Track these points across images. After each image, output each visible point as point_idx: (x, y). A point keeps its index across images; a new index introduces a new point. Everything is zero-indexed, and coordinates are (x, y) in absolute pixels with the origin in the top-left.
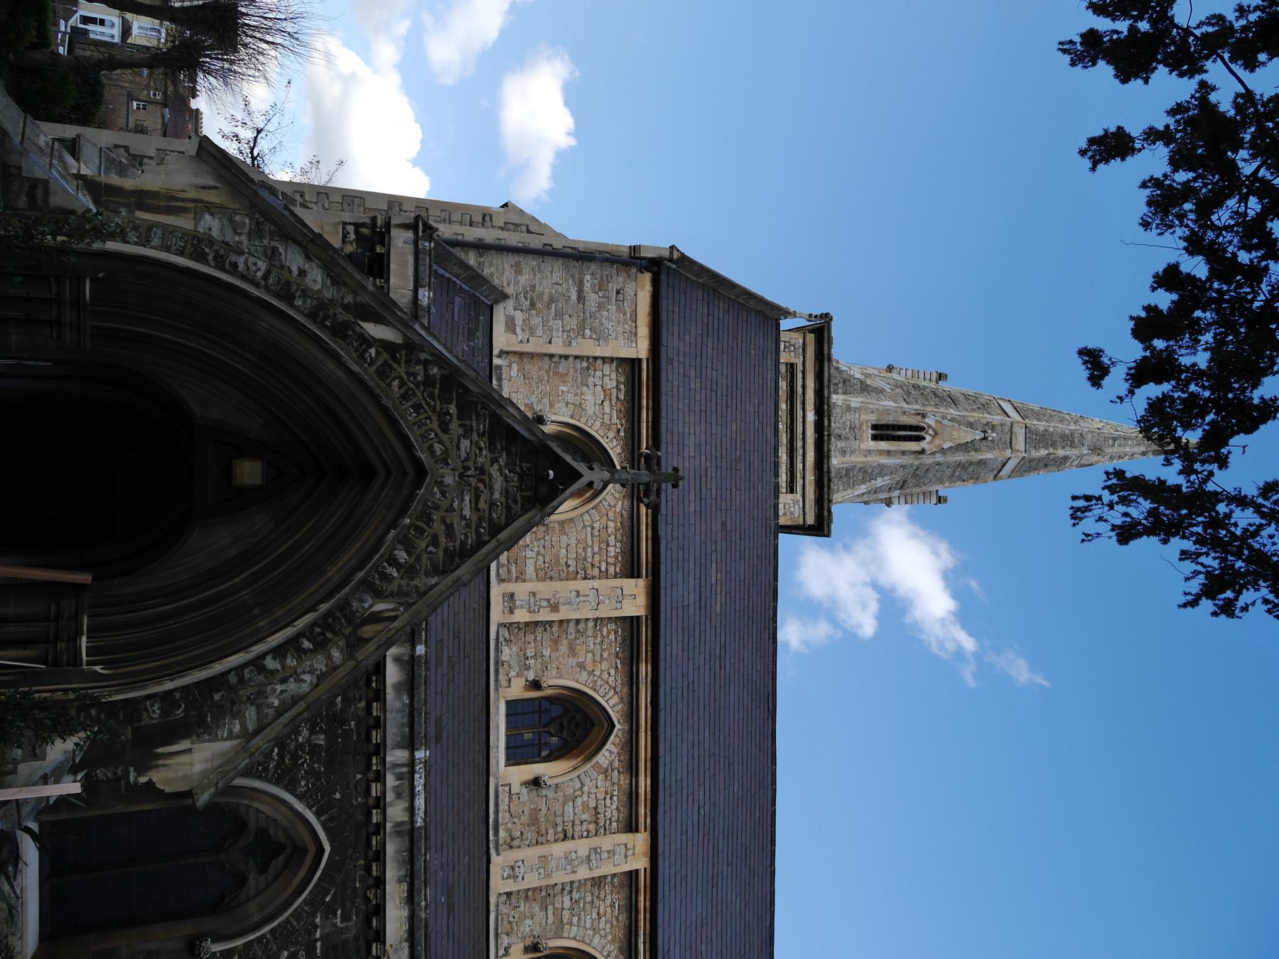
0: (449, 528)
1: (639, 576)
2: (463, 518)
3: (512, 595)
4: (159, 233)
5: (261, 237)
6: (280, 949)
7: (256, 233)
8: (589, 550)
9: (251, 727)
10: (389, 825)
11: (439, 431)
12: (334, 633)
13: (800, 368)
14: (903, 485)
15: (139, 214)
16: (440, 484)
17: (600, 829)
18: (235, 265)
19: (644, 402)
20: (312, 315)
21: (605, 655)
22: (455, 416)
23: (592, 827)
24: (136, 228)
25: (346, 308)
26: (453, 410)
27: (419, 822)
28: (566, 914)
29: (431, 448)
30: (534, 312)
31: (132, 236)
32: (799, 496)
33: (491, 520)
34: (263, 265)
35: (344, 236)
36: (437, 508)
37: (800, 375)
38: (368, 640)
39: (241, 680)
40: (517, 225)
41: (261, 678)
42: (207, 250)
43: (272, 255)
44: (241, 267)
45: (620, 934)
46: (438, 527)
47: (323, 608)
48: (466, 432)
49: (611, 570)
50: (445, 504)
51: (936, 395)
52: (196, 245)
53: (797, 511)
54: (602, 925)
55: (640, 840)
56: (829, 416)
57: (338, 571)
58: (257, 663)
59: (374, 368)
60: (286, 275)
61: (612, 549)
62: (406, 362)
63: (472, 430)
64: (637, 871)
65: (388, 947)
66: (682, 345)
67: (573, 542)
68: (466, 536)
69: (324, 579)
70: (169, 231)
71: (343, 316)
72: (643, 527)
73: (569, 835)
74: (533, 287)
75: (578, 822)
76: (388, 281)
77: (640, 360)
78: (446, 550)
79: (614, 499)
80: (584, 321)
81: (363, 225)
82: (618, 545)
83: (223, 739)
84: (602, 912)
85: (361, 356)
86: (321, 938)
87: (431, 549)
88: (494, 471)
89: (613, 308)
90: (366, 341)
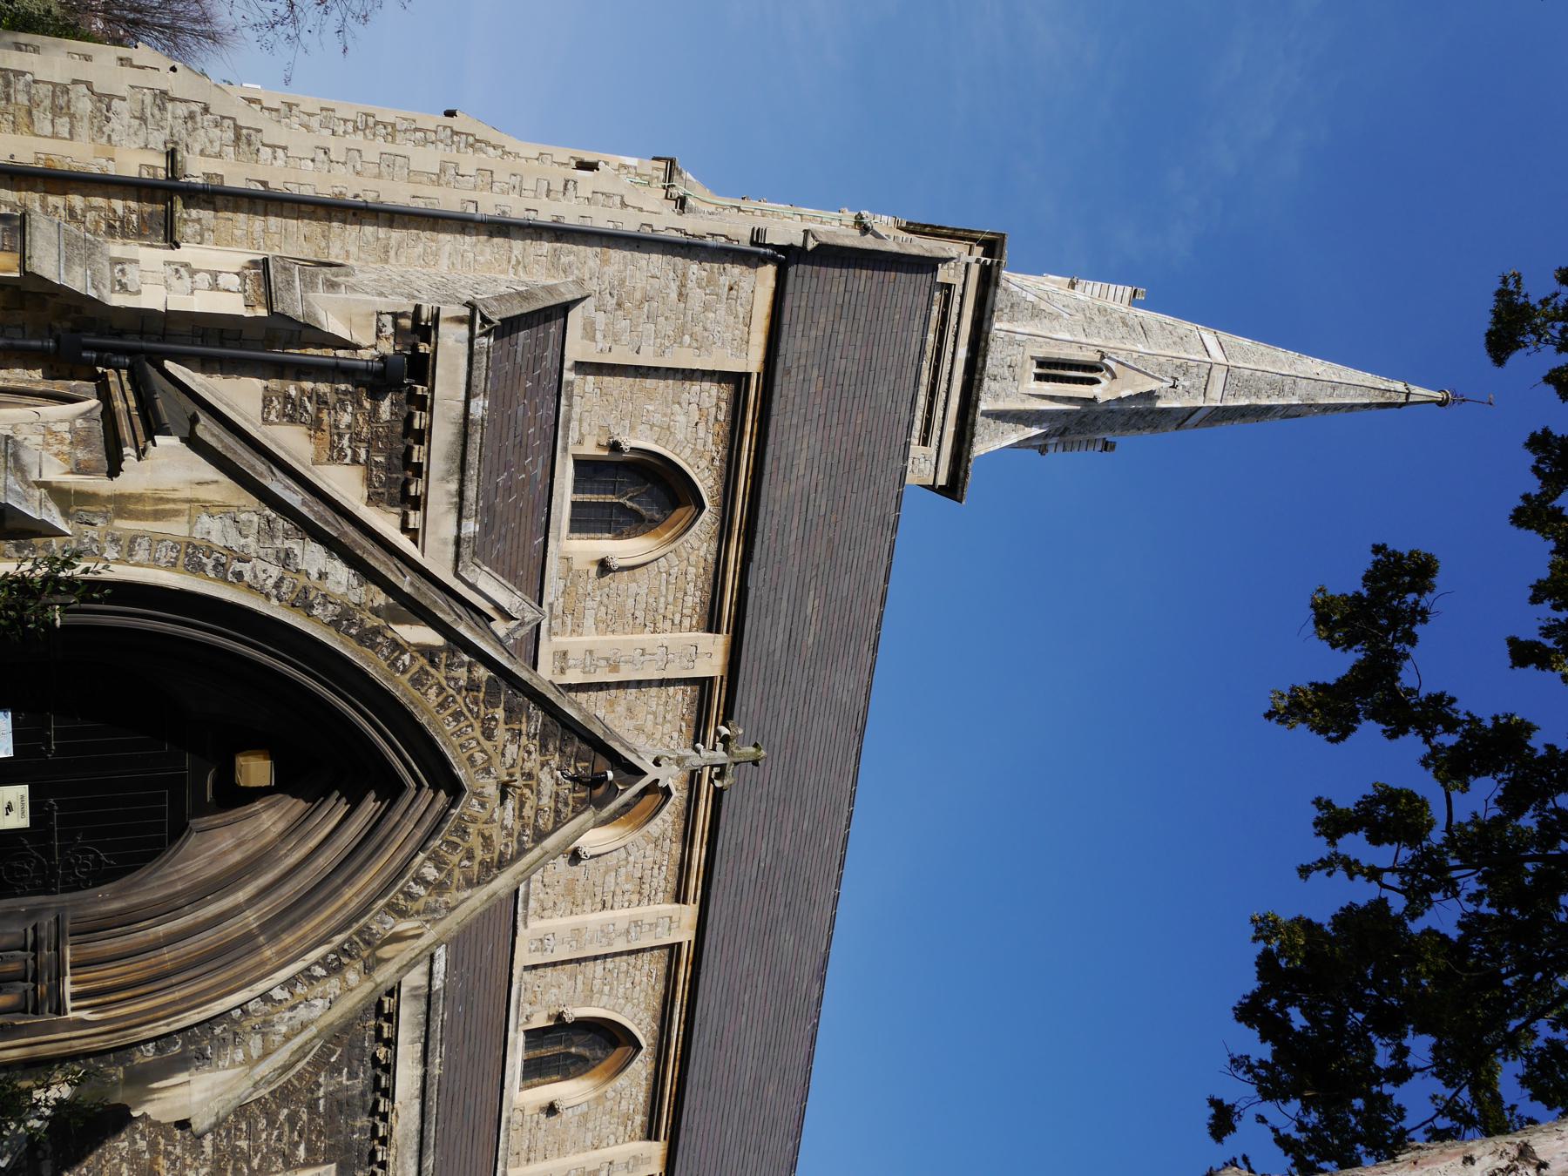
0: (487, 841)
1: (718, 631)
2: (504, 827)
3: (565, 653)
4: (145, 544)
5: (273, 537)
6: (279, 1107)
7: (268, 531)
8: (662, 600)
9: (255, 1054)
10: (403, 990)
11: (481, 739)
12: (350, 956)
13: (959, 290)
14: (1063, 432)
15: (119, 523)
16: (478, 795)
17: (642, 893)
18: (239, 575)
19: (748, 428)
20: (335, 624)
21: (669, 717)
22: (501, 721)
23: (635, 897)
24: (115, 541)
25: (376, 612)
26: (500, 714)
27: (438, 984)
28: (597, 982)
29: (471, 759)
30: (620, 313)
31: (111, 553)
32: (932, 450)
33: (536, 827)
34: (275, 572)
35: (379, 331)
36: (474, 820)
37: (957, 299)
38: (387, 960)
39: (245, 1013)
40: (607, 195)
41: (268, 1007)
42: (205, 560)
43: (285, 559)
44: (247, 577)
45: (656, 1003)
46: (475, 841)
47: (338, 939)
48: (513, 737)
49: (686, 622)
50: (484, 815)
51: (1125, 324)
52: (192, 555)
53: (928, 468)
54: (636, 995)
55: (690, 912)
56: (985, 356)
57: (356, 895)
58: (265, 997)
59: (408, 676)
60: (303, 580)
61: (689, 599)
62: (447, 666)
63: (520, 734)
64: (680, 944)
65: (397, 1105)
66: (805, 344)
67: (643, 591)
68: (506, 845)
69: (340, 902)
70: (156, 540)
71: (373, 622)
72: (730, 576)
73: (608, 905)
74: (622, 282)
75: (619, 892)
76: (432, 390)
77: (748, 375)
78: (481, 863)
79: (699, 539)
80: (683, 325)
81: (404, 315)
82: (698, 593)
83: (224, 1068)
84: (637, 980)
85: (393, 664)
86: (325, 1096)
87: (465, 863)
88: (544, 776)
89: (722, 307)
90: (398, 646)
